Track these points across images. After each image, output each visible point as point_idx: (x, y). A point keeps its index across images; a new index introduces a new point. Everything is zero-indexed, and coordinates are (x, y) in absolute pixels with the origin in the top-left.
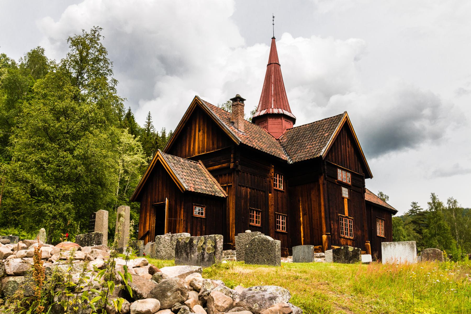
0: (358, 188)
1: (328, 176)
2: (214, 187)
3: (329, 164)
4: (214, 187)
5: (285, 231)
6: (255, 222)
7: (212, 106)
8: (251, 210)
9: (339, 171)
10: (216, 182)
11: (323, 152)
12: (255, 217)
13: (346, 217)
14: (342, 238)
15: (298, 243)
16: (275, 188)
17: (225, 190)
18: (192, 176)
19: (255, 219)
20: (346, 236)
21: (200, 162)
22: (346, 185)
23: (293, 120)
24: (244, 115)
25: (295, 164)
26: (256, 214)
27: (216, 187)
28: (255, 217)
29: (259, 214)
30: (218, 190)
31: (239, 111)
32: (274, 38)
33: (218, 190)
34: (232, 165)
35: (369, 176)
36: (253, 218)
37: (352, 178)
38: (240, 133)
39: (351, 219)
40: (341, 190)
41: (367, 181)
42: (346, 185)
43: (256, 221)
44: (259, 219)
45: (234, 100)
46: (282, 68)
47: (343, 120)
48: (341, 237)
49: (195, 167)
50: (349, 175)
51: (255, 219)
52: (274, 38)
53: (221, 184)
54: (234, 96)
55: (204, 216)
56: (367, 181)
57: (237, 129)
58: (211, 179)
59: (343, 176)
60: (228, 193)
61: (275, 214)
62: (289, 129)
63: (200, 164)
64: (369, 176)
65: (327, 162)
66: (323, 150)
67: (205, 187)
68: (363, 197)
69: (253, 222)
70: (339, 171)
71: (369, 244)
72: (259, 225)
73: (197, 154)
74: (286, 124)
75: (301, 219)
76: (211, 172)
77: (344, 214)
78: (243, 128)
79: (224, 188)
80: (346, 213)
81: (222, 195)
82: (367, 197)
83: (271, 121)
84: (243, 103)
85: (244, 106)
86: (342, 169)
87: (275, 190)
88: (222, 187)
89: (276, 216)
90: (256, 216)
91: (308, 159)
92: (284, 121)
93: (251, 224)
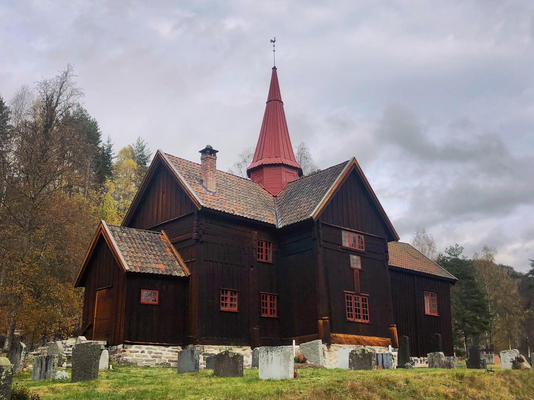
6: (269, 311)
7: (179, 161)
9: (344, 234)
12: (269, 304)
16: (260, 260)
22: (356, 253)
28: (269, 304)
31: (209, 166)
32: (274, 69)
39: (366, 296)
43: (271, 310)
45: (203, 152)
51: (269, 308)
52: (274, 69)
53: (184, 260)
55: (157, 303)
57: (206, 189)
61: (260, 294)
63: (162, 234)
69: (266, 313)
71: (395, 329)
72: (275, 316)
78: (214, 186)
85: (216, 159)
87: (259, 262)
91: (297, 222)
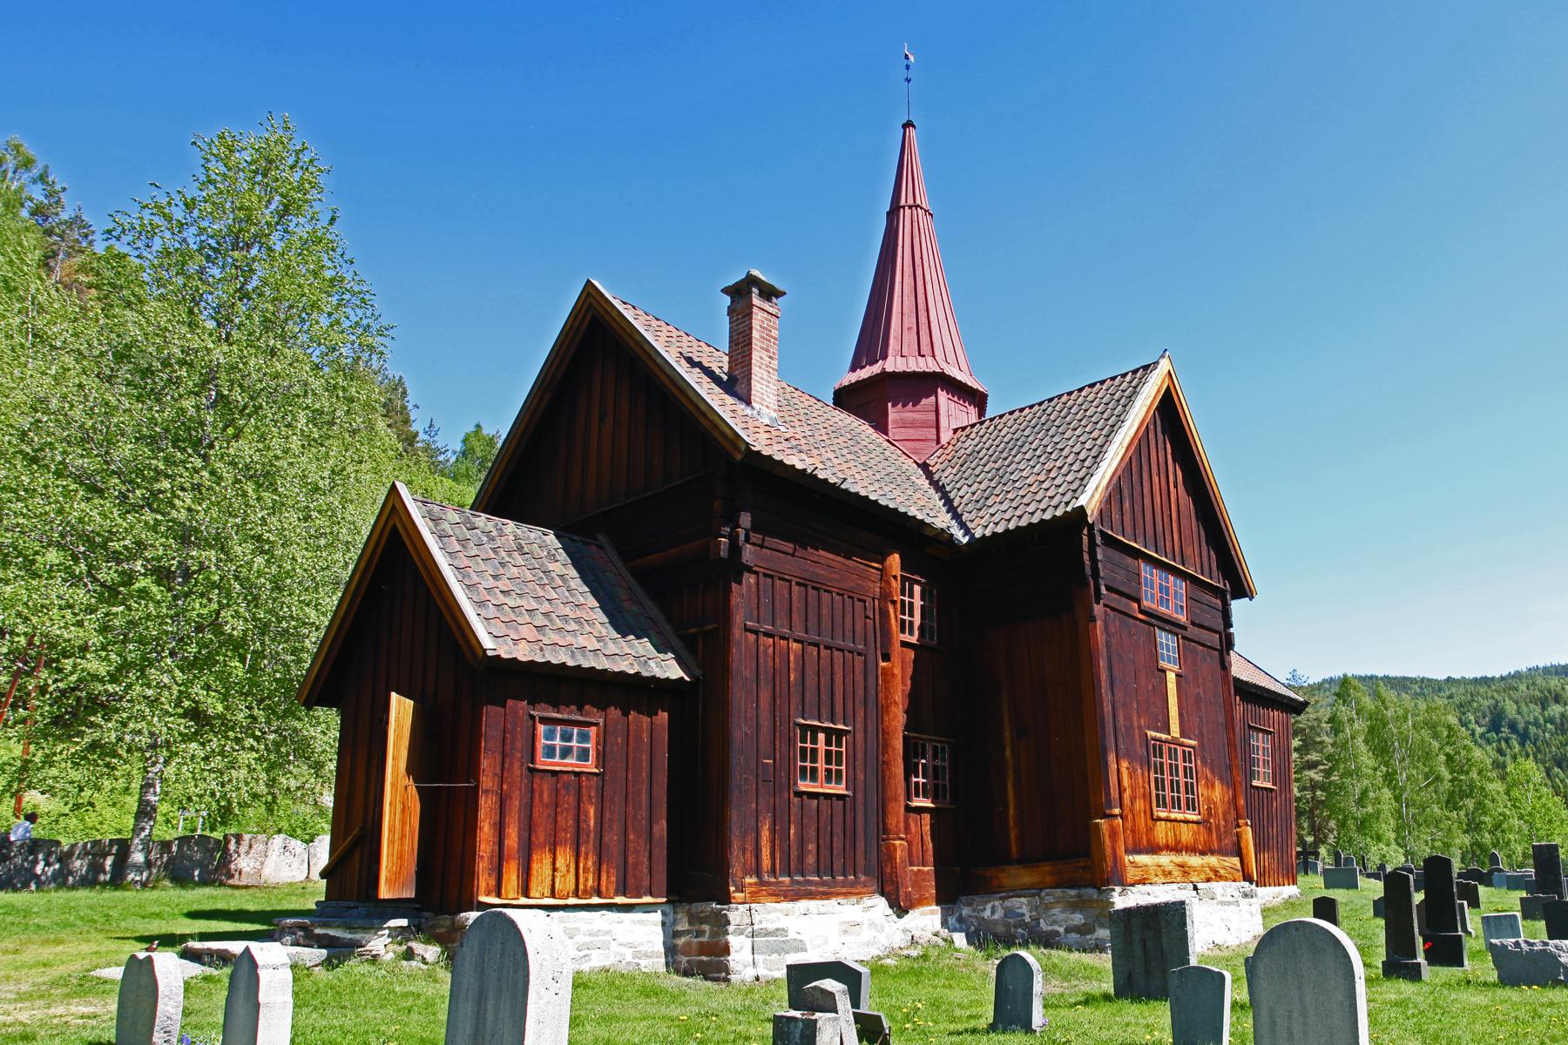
1: (1108, 588)
6: (821, 774)
8: (804, 728)
9: (394, 695)
11: (1091, 498)
12: (821, 755)
13: (1175, 742)
14: (1160, 819)
15: (1004, 860)
19: (821, 765)
21: (602, 538)
26: (828, 743)
29: (839, 745)
35: (1241, 589)
36: (814, 760)
41: (1237, 606)
44: (839, 763)
51: (821, 765)
62: (964, 429)
64: (1241, 589)
65: (1103, 533)
66: (1092, 483)
68: (1225, 666)
72: (840, 789)
75: (1008, 753)
88: (682, 638)
90: (828, 753)
93: (804, 786)
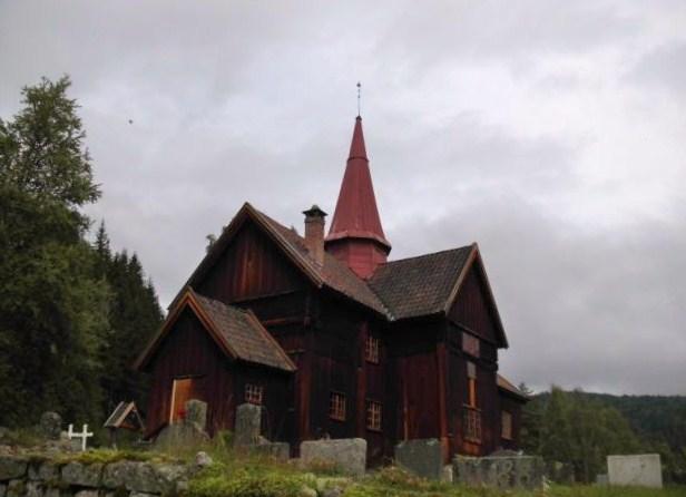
0: (488, 364)
2: (276, 356)
3: (452, 324)
4: (276, 356)
5: (378, 428)
9: (465, 335)
10: (279, 347)
17: (293, 359)
18: (245, 337)
20: (473, 440)
21: (249, 310)
22: (472, 359)
23: (386, 249)
24: (495, 338)
25: (399, 322)
27: (278, 354)
30: (281, 358)
32: (359, 119)
33: (281, 358)
34: (307, 320)
35: (504, 344)
37: (482, 350)
38: (318, 266)
40: (466, 367)
41: (501, 352)
42: (472, 359)
46: (630, 394)
47: (471, 256)
48: (465, 441)
49: (245, 320)
50: (477, 342)
52: (359, 119)
54: (309, 208)
56: (501, 352)
58: (270, 341)
59: (470, 345)
60: (298, 365)
64: (504, 344)
67: (264, 353)
70: (465, 335)
73: (243, 299)
74: (376, 254)
76: (269, 328)
77: (469, 404)
79: (292, 356)
80: (473, 405)
81: (289, 368)
82: (499, 382)
83: (352, 248)
84: (323, 219)
86: (469, 333)
88: (288, 354)
89: (368, 405)
92: (374, 251)
